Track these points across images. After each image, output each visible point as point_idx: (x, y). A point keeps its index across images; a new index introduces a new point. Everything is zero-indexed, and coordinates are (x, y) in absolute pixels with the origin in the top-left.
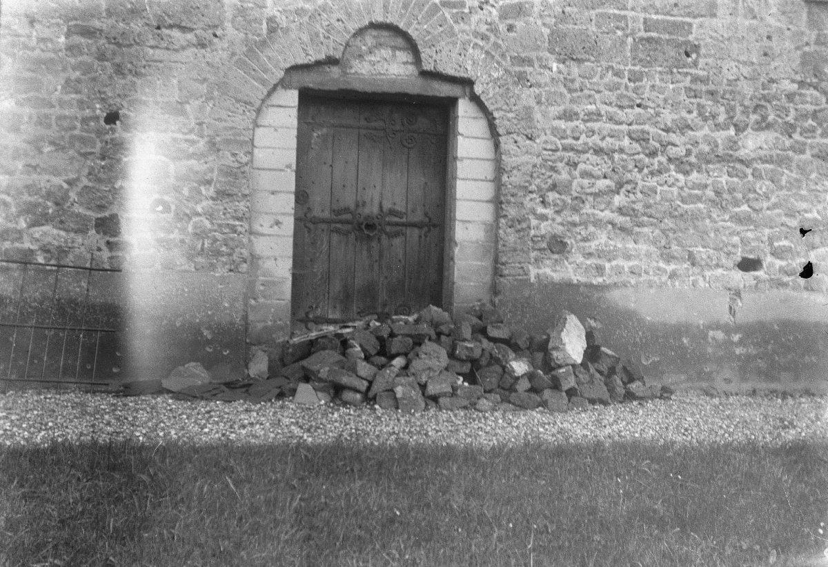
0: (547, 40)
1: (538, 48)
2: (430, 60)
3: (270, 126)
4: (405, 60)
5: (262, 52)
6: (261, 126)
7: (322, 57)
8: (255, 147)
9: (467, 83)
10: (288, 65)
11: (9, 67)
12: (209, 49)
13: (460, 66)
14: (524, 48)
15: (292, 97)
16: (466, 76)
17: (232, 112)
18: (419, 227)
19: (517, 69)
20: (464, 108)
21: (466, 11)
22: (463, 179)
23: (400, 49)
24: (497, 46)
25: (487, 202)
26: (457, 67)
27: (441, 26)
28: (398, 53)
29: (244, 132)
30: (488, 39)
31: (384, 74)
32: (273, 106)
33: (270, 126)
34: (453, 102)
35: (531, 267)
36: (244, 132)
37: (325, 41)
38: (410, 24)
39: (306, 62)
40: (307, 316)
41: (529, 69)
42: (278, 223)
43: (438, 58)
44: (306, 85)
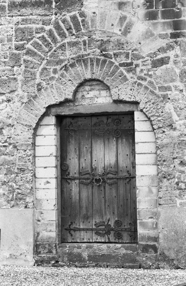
0: (179, 76)
1: (173, 80)
2: (116, 94)
3: (42, 135)
4: (105, 95)
5: (35, 101)
6: (38, 135)
7: (62, 99)
8: (36, 146)
9: (137, 103)
10: (47, 106)
11: (120, 1)
12: (11, 102)
13: (132, 96)
14: (165, 81)
15: (51, 120)
16: (134, 100)
17: (23, 131)
18: (86, 185)
19: (162, 93)
20: (137, 115)
21: (134, 66)
22: (139, 154)
23: (102, 90)
24: (151, 83)
25: (153, 165)
26: (130, 96)
27: (120, 76)
28: (102, 92)
29: (29, 140)
30: (146, 80)
31: (96, 104)
32: (43, 125)
33: (42, 135)
34: (132, 114)
35: (176, 199)
36: (29, 140)
37: (64, 91)
38: (104, 78)
39: (55, 103)
40: (70, 227)
41: (169, 93)
42: (48, 182)
43: (119, 93)
44: (59, 114)
